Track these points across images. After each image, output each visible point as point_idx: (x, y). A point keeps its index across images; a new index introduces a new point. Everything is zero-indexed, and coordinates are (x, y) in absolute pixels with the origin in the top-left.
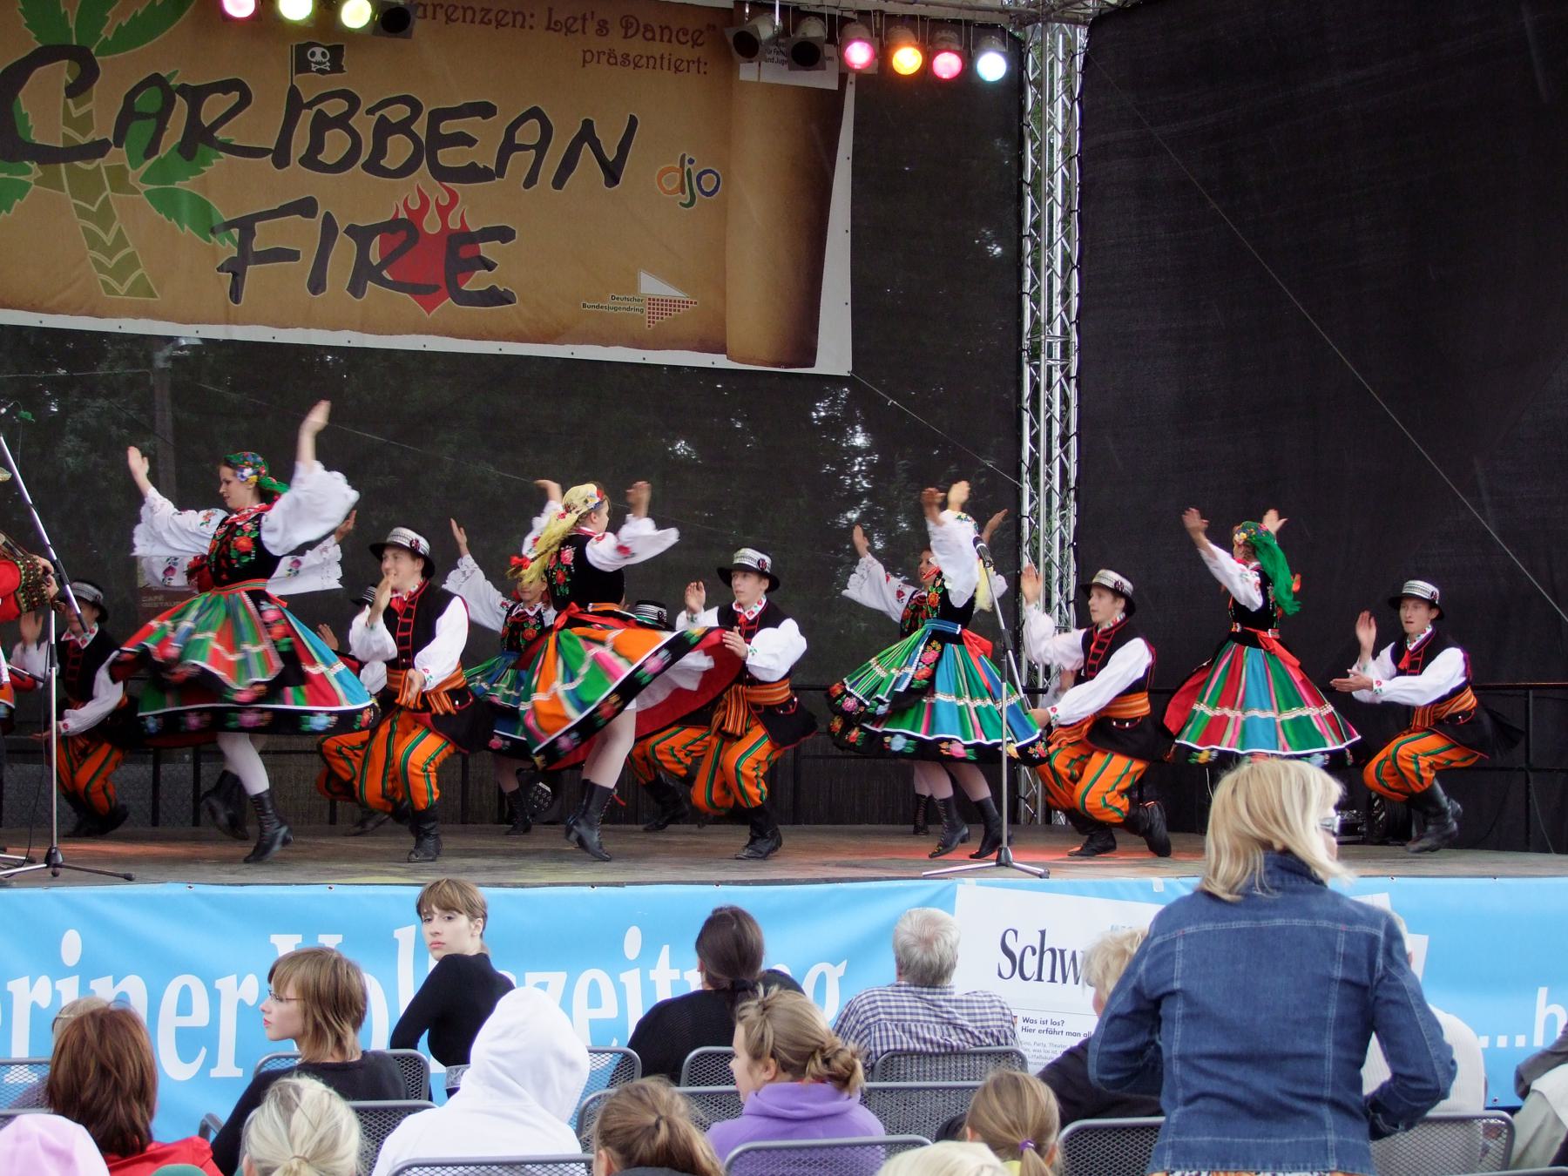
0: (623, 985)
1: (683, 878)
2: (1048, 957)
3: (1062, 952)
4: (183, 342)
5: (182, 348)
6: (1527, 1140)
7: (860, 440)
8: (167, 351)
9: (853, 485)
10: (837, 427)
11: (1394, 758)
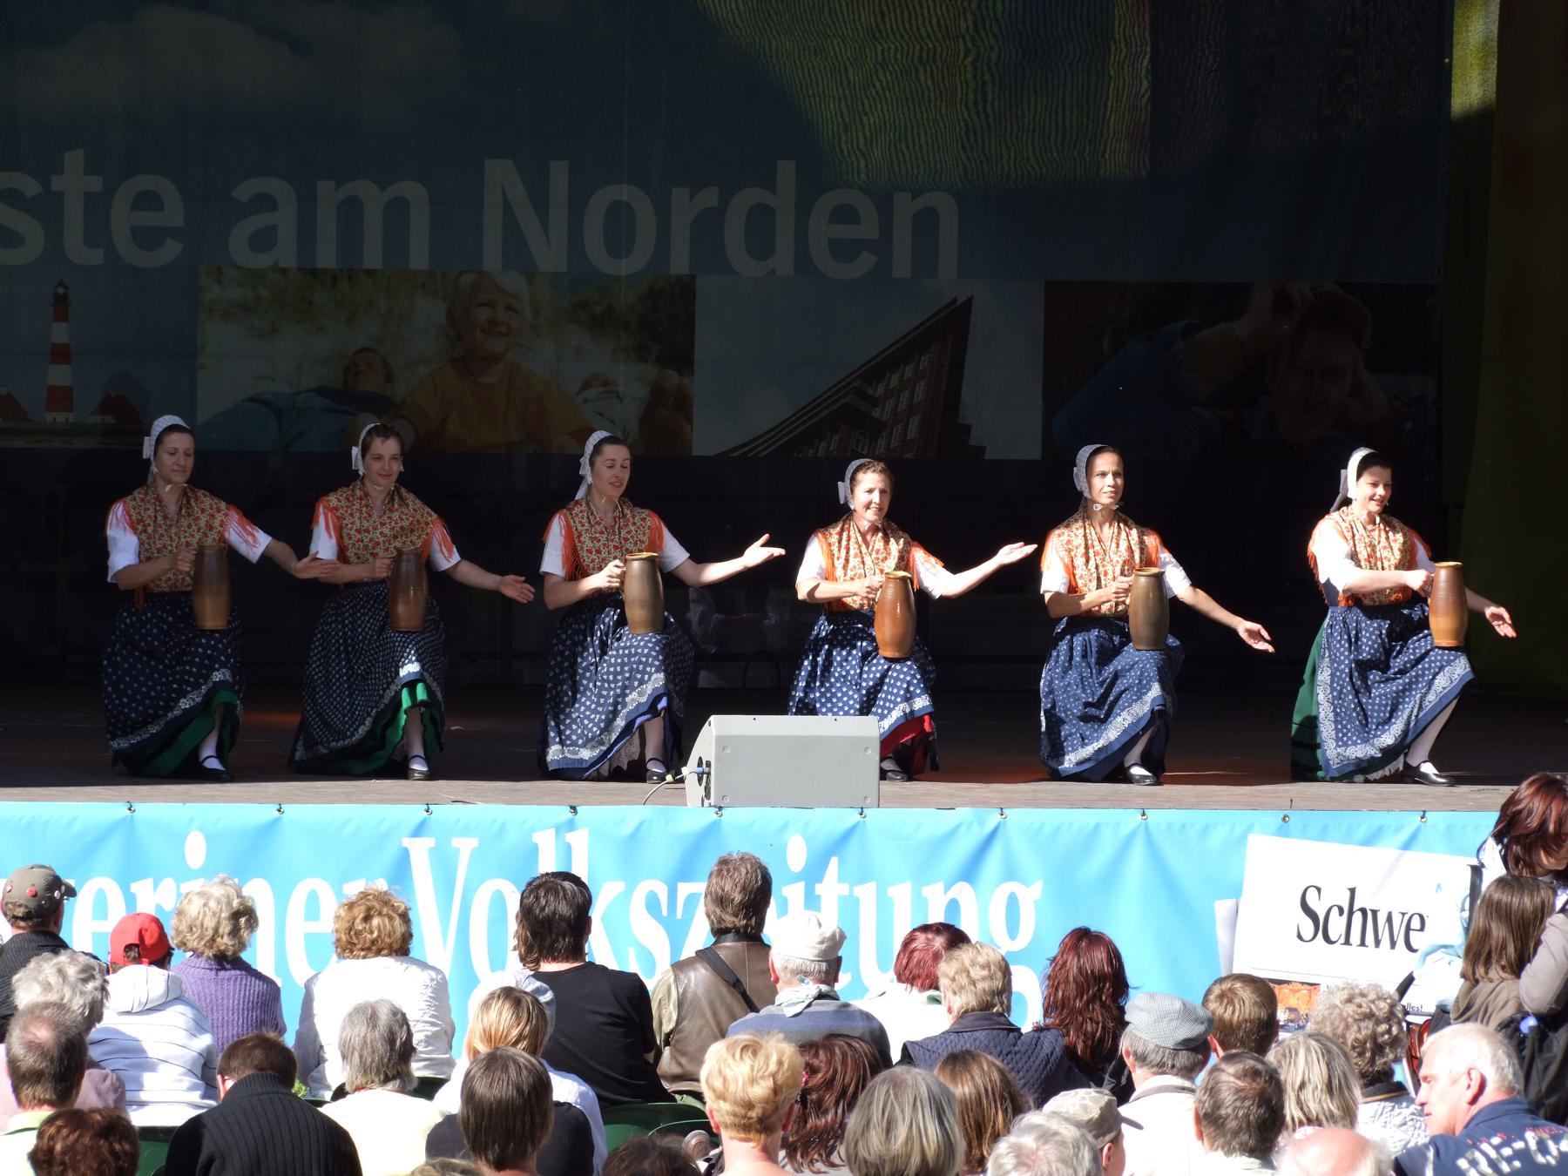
0: (134, 895)
2: (1357, 917)
3: (1375, 913)
6: (298, 1013)
11: (204, 1097)
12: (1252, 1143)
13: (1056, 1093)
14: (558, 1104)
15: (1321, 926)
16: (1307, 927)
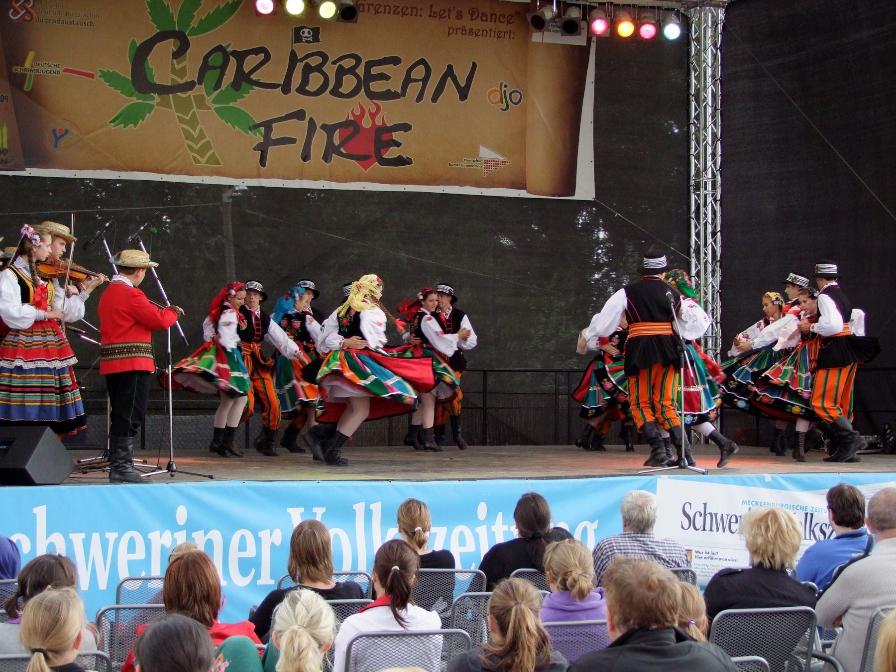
1: (508, 476)
2: (708, 517)
3: (716, 515)
4: (237, 189)
5: (237, 192)
7: (602, 235)
8: (229, 193)
9: (597, 259)
10: (589, 229)
12: (379, 294)
13: (154, 45)
14: (521, 532)
15: (692, 522)
16: (686, 523)
